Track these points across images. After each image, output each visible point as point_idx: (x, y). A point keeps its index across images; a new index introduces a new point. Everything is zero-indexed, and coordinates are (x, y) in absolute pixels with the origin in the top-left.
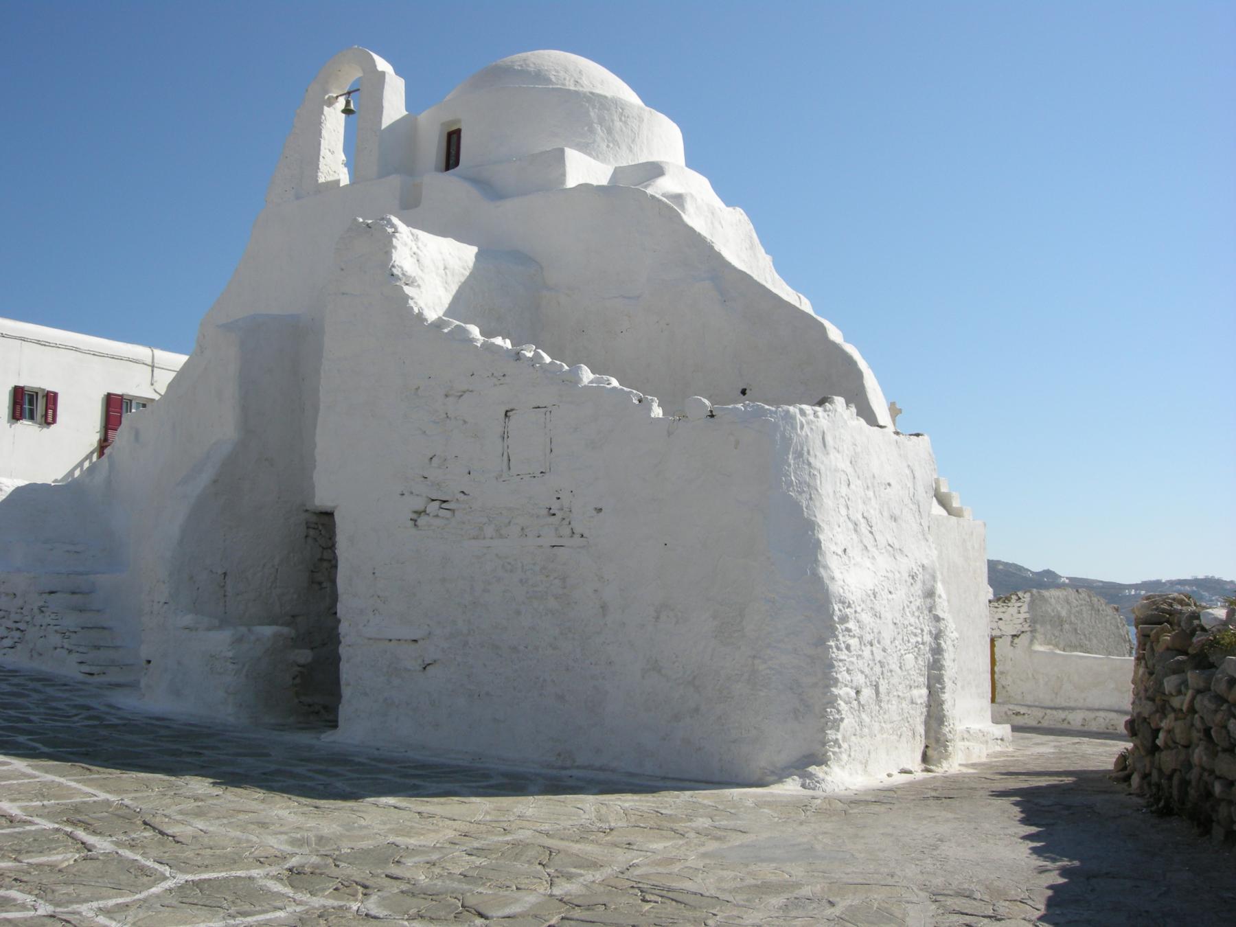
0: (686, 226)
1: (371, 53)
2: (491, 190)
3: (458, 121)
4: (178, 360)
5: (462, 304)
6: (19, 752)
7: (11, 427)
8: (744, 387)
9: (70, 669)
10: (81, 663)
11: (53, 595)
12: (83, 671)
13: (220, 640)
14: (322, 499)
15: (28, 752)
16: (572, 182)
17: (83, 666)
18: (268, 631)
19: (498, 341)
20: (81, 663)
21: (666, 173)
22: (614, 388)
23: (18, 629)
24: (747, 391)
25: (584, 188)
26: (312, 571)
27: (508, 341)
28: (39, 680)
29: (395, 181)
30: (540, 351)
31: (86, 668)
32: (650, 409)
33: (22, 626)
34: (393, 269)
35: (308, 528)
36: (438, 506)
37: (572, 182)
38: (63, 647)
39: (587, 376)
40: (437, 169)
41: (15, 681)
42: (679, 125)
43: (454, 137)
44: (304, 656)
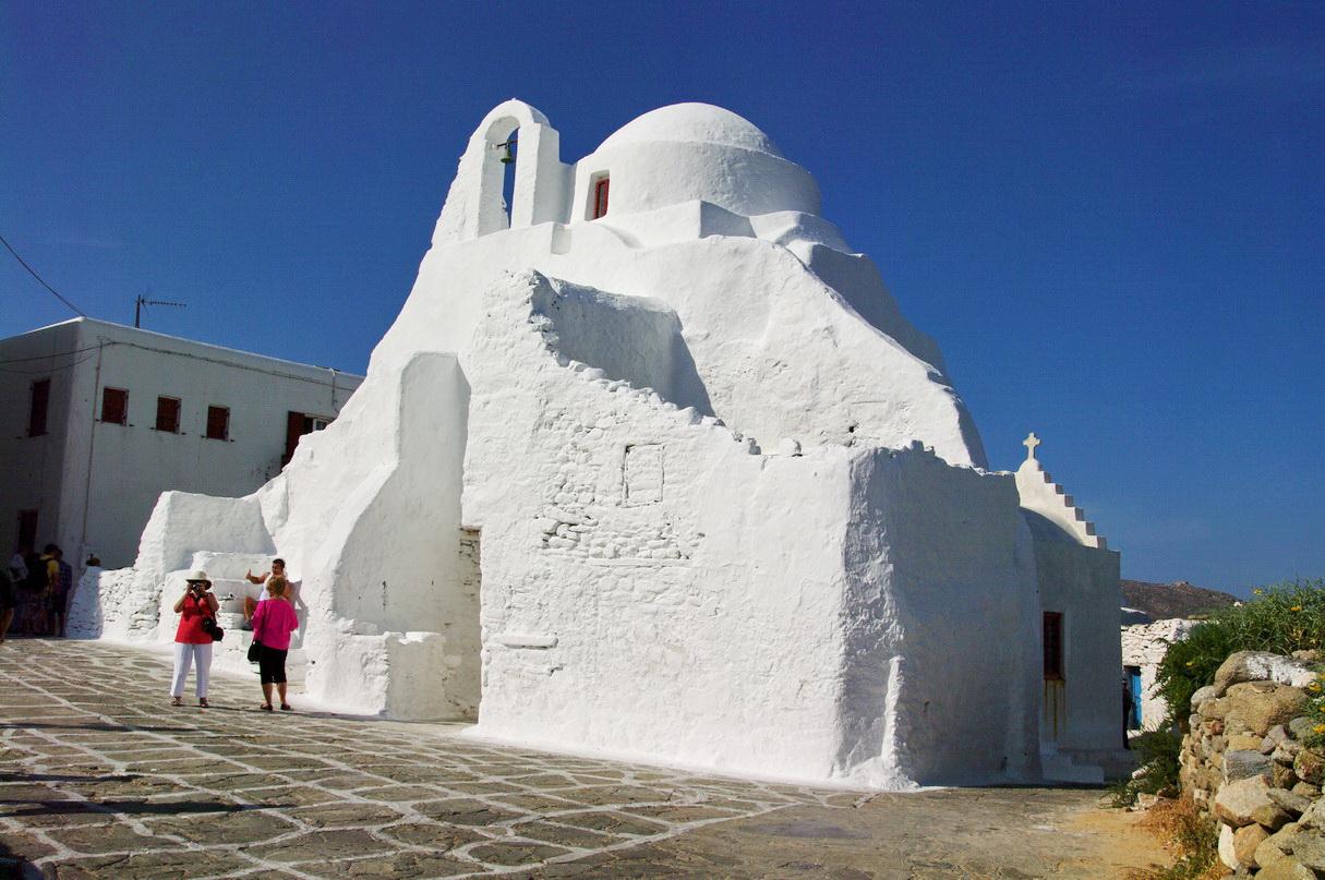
35: (462, 544)
43: (603, 190)
44: (456, 660)
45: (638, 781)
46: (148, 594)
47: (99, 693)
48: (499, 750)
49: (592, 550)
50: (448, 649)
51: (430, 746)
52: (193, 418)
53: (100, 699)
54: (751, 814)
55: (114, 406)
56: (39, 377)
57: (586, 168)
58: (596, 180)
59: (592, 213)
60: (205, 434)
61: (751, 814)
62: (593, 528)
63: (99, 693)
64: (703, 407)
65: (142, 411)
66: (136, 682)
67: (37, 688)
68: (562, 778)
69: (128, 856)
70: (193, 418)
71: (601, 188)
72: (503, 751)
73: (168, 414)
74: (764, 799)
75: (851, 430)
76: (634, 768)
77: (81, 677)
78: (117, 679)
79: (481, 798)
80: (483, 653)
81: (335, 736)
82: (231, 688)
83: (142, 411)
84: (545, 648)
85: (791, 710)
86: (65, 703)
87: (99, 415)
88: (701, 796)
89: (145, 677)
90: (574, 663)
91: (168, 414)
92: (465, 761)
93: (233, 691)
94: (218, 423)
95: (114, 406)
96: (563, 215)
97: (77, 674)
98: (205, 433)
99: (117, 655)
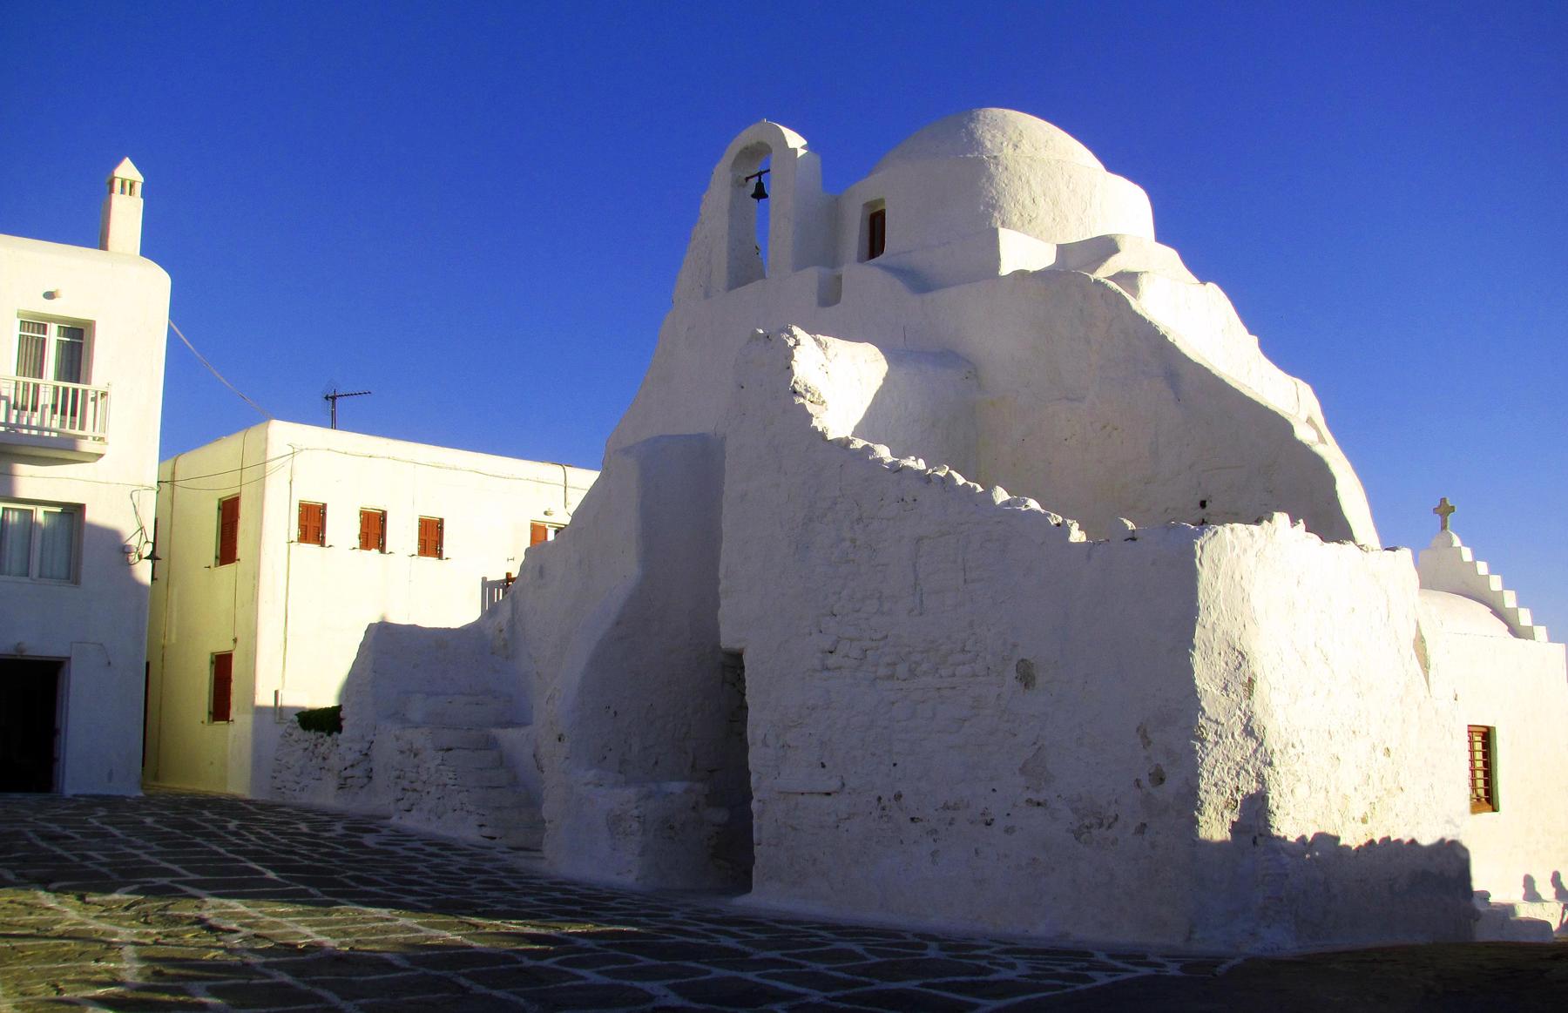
0: (1134, 313)
1: (781, 127)
2: (919, 282)
3: (882, 201)
4: (591, 476)
5: (871, 424)
6: (464, 951)
8: (1203, 499)
9: (468, 832)
10: (481, 826)
11: (450, 752)
12: (484, 834)
13: (624, 798)
14: (728, 641)
15: (368, 888)
16: (1006, 269)
17: (484, 829)
18: (676, 787)
19: (910, 462)
20: (481, 826)
21: (1121, 246)
22: (1031, 511)
23: (415, 790)
24: (1207, 503)
25: (1021, 275)
26: (731, 721)
27: (921, 461)
28: (436, 845)
29: (812, 275)
30: (953, 472)
31: (487, 831)
32: (1068, 533)
33: (418, 786)
34: (796, 385)
37: (1006, 269)
38: (462, 809)
39: (1001, 495)
40: (860, 260)
41: (409, 845)
42: (455, 629)
44: (721, 816)
45: (945, 953)
46: (357, 747)
47: (306, 862)
48: (775, 921)
49: (882, 671)
51: (690, 918)
52: (403, 535)
53: (307, 869)
54: (1082, 987)
55: (313, 524)
56: (227, 493)
57: (868, 189)
58: (869, 213)
59: (866, 251)
60: (416, 553)
61: (1082, 987)
62: (882, 643)
63: (306, 862)
64: (1326, 443)
65: (343, 527)
66: (348, 850)
67: (538, 903)
68: (851, 951)
69: (76, 975)
70: (403, 535)
71: (876, 225)
72: (781, 922)
73: (373, 530)
74: (1102, 970)
75: (1203, 504)
76: (941, 937)
77: (286, 845)
78: (328, 847)
79: (751, 976)
80: (754, 805)
81: (578, 908)
82: (459, 855)
83: (343, 527)
84: (829, 794)
85: (791, 826)
86: (271, 875)
87: (294, 536)
88: (1022, 968)
89: (362, 845)
90: (404, 778)
91: (373, 530)
92: (733, 935)
93: (459, 858)
94: (431, 538)
95: (313, 524)
96: (830, 258)
97: (283, 841)
98: (415, 548)
99: (326, 818)
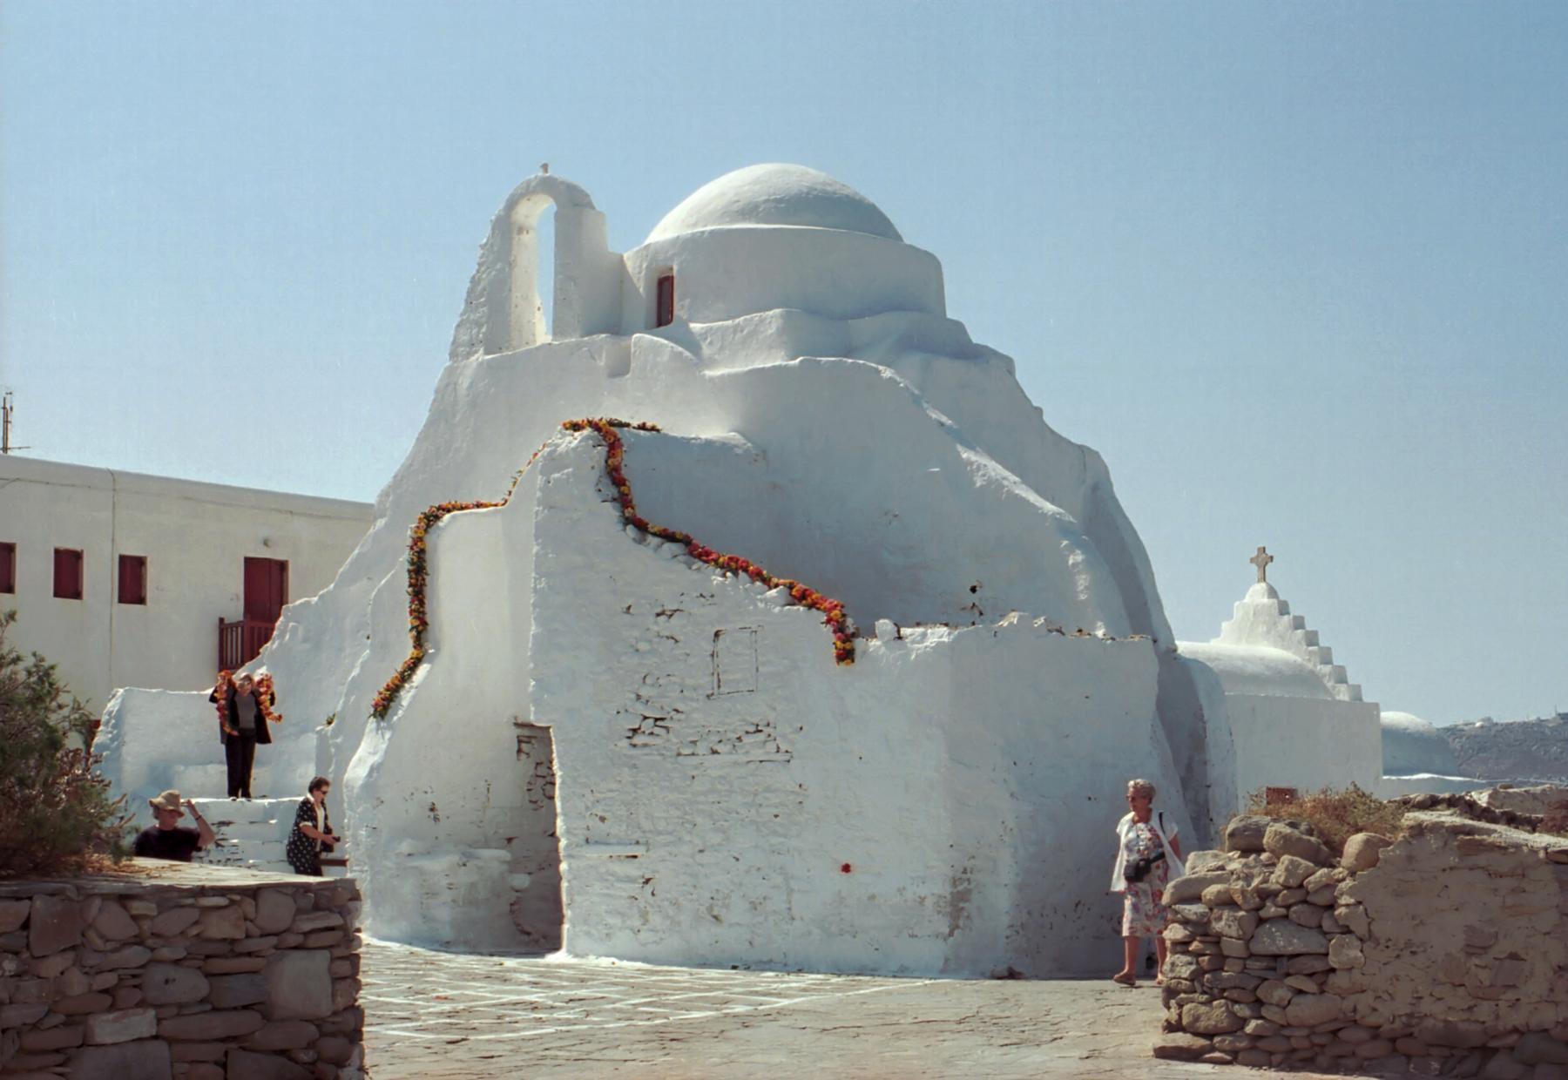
7: (1252, 560)
36: (652, 725)
44: (522, 881)
50: (514, 866)
70: (99, 576)
